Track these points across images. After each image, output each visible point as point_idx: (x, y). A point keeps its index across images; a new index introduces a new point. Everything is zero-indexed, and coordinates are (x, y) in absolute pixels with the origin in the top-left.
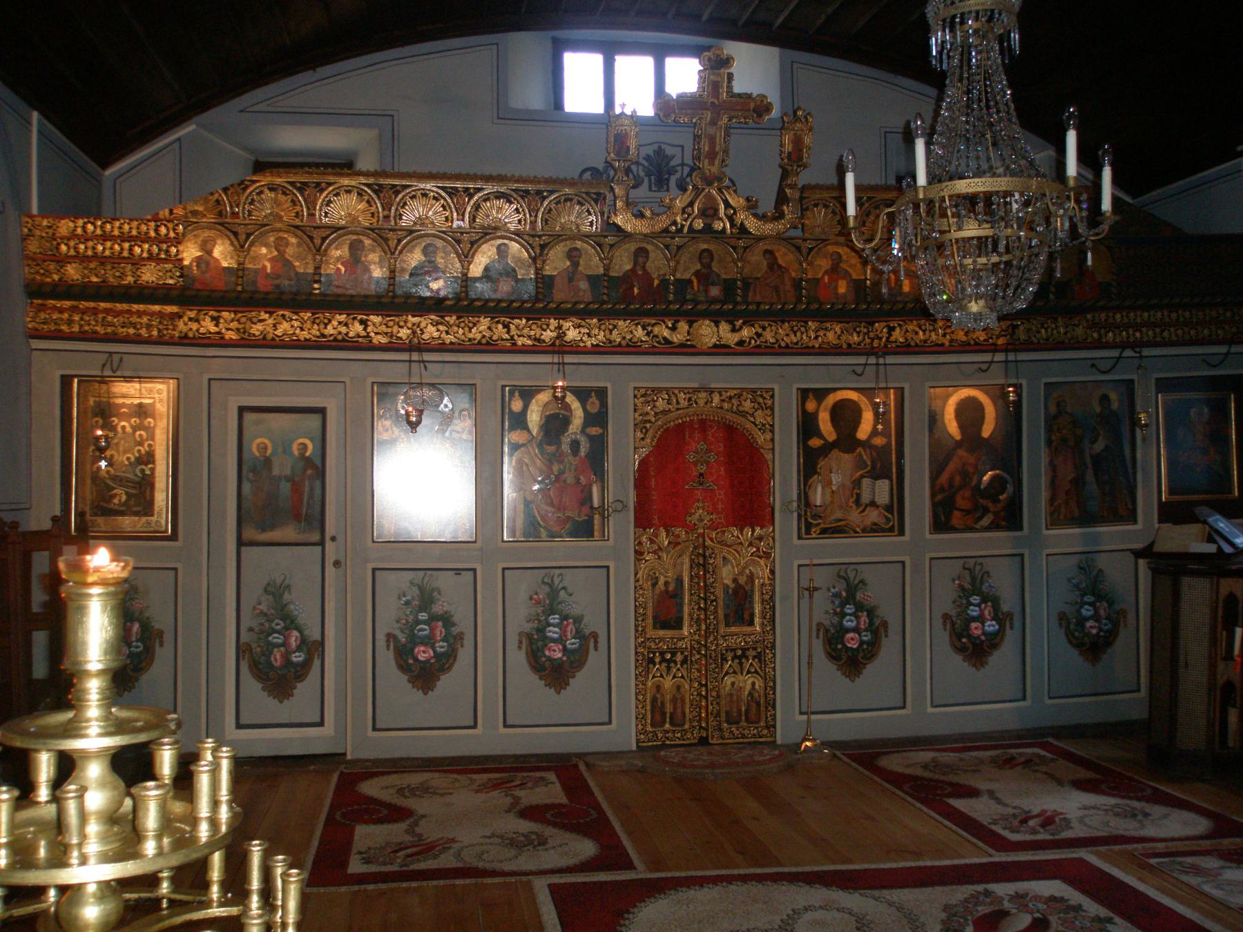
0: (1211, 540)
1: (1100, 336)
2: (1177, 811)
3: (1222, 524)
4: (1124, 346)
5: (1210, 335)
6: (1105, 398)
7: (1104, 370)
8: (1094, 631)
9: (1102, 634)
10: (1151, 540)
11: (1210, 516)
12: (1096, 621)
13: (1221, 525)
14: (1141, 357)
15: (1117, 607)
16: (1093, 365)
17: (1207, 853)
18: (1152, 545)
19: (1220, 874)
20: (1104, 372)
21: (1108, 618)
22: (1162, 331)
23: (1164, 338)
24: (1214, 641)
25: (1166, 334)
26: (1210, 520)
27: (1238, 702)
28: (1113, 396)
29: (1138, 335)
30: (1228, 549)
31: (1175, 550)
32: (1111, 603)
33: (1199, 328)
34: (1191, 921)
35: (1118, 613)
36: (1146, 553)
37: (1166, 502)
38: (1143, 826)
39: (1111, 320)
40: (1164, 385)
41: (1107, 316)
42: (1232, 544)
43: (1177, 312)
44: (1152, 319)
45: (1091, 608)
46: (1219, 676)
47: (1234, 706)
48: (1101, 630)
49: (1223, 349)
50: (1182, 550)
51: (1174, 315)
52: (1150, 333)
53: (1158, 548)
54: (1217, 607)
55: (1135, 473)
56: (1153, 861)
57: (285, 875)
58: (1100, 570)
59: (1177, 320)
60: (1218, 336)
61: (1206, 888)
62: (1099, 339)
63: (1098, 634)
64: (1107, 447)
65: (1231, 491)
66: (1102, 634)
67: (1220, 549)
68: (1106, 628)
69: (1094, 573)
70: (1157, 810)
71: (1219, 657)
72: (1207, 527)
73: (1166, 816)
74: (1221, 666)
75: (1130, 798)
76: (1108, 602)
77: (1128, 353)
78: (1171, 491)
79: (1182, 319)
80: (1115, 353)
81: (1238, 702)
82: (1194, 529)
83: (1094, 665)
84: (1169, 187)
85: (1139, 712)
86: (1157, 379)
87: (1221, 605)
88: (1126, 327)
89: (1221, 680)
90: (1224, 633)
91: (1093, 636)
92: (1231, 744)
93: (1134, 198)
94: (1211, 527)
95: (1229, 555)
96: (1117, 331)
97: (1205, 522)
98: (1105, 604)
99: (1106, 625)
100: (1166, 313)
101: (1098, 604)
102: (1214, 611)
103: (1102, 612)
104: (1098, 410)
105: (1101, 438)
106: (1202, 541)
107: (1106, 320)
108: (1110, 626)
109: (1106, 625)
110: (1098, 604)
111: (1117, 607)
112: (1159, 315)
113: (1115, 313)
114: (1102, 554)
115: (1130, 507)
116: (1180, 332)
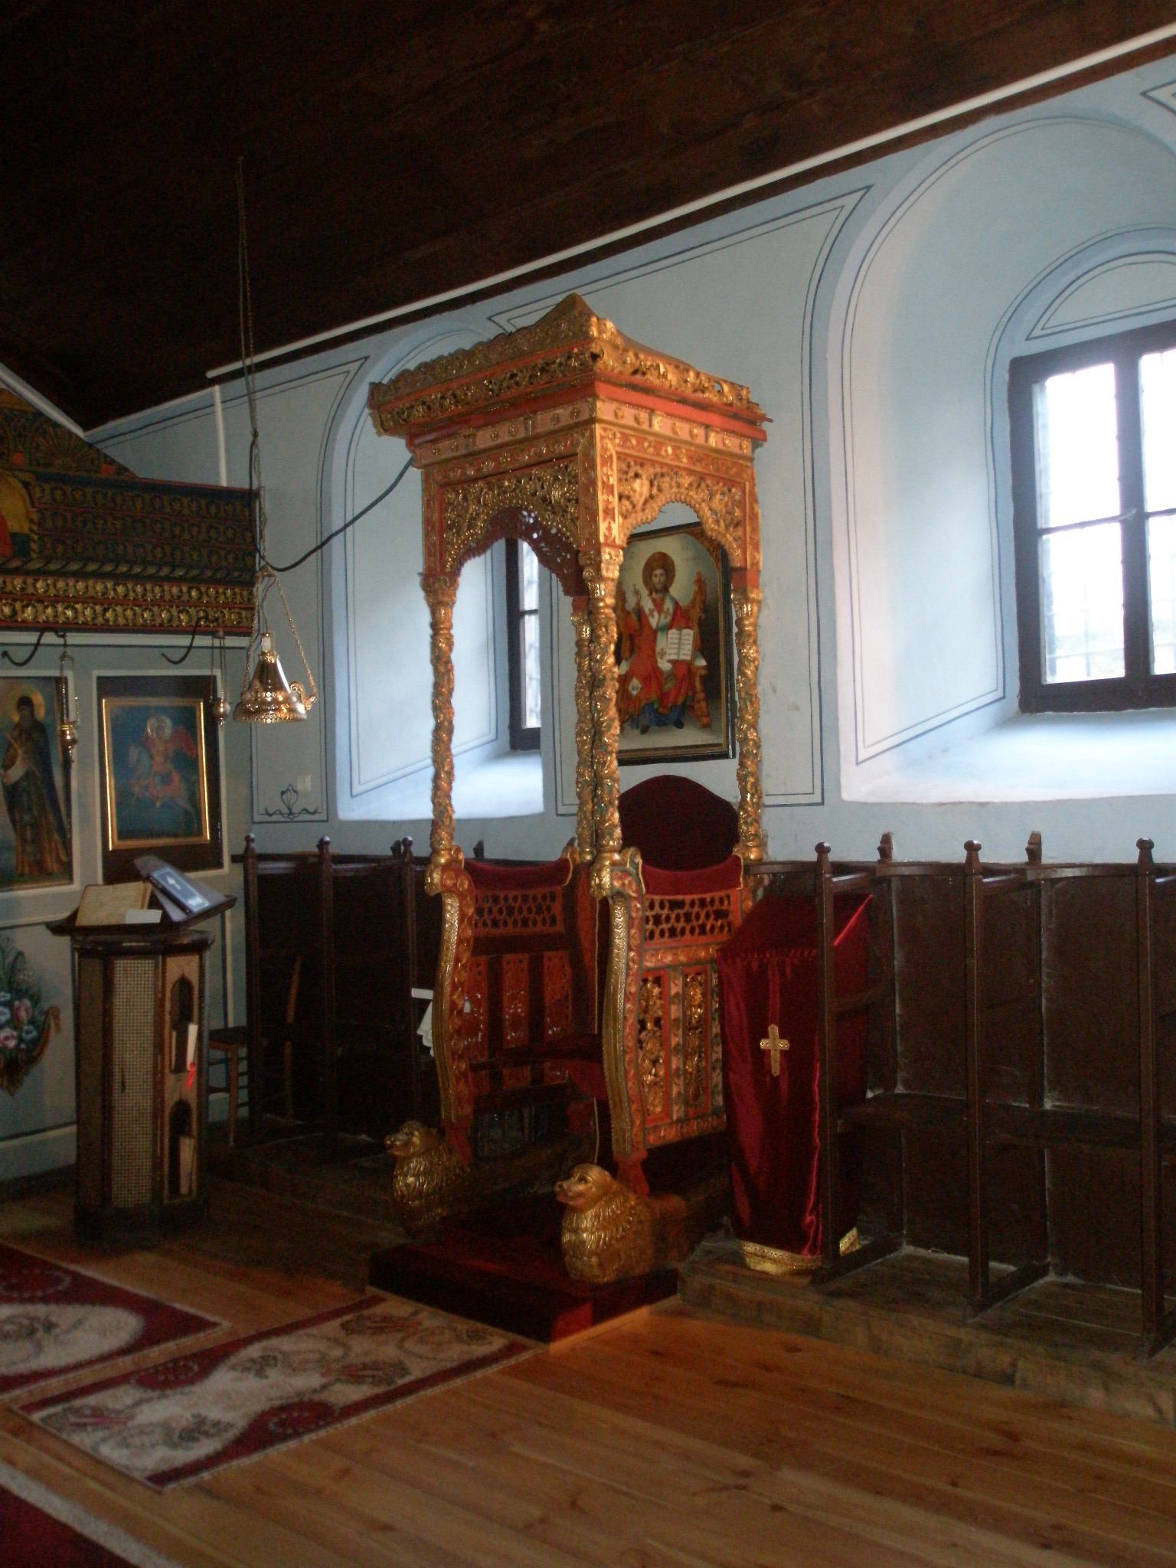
0: (154, 903)
1: (14, 612)
2: (98, 1309)
3: (172, 880)
4: (44, 628)
5: (170, 621)
6: (25, 702)
7: (17, 661)
8: (12, 1044)
9: (23, 1046)
10: (77, 906)
11: (156, 868)
12: (15, 1028)
13: (171, 881)
14: (65, 645)
15: (45, 1005)
16: (5, 654)
17: (122, 1380)
18: (74, 916)
19: (132, 1417)
20: (20, 665)
21: (32, 1022)
22: (106, 610)
23: (107, 621)
24: (159, 1046)
25: (109, 615)
26: (156, 875)
27: (195, 1133)
28: (38, 699)
29: (69, 613)
30: (177, 915)
31: (105, 922)
32: (36, 1000)
33: (156, 609)
34: (65, 1527)
35: (47, 1014)
36: (64, 927)
37: (113, 851)
38: (39, 1348)
39: (31, 590)
40: (108, 687)
41: (25, 582)
42: (182, 907)
43: (125, 585)
44: (91, 592)
45: (6, 1010)
46: (167, 1096)
47: (189, 1135)
48: (21, 1040)
49: (184, 640)
50: (113, 921)
51: (120, 589)
52: (88, 612)
53: (83, 921)
54: (163, 1000)
55: (69, 815)
56: (36, 1417)
57: (170, 1033)
58: (20, 954)
59: (126, 596)
60: (180, 621)
61: (107, 1451)
62: (12, 617)
63: (17, 1046)
64: (27, 775)
65: (200, 832)
66: (23, 1046)
67: (165, 916)
68: (28, 1037)
69: (10, 959)
70: (65, 1315)
71: (167, 1071)
72: (150, 887)
73: (78, 1324)
74: (170, 1080)
75: (32, 1300)
76: (31, 998)
77: (50, 638)
78: (122, 835)
79: (132, 595)
80: (31, 638)
81: (195, 1133)
82: (133, 890)
83: (12, 1095)
84: (133, 417)
85: (67, 1155)
86: (99, 678)
87: (168, 994)
88: (55, 601)
89: (170, 1099)
90: (174, 1034)
91: (11, 1050)
92: (184, 1190)
93: (86, 427)
94: (155, 885)
95: (178, 924)
96: (40, 607)
97: (148, 879)
98: (27, 1002)
99: (28, 1032)
100: (110, 585)
101: (17, 1003)
102: (160, 1003)
103: (23, 1014)
104: (16, 719)
105: (18, 762)
106: (142, 907)
107: (22, 589)
108: (35, 1033)
109: (28, 1032)
110: (17, 1003)
111: (45, 1005)
112: (99, 587)
113: (37, 580)
114: (22, 930)
115: (64, 858)
116: (129, 613)
